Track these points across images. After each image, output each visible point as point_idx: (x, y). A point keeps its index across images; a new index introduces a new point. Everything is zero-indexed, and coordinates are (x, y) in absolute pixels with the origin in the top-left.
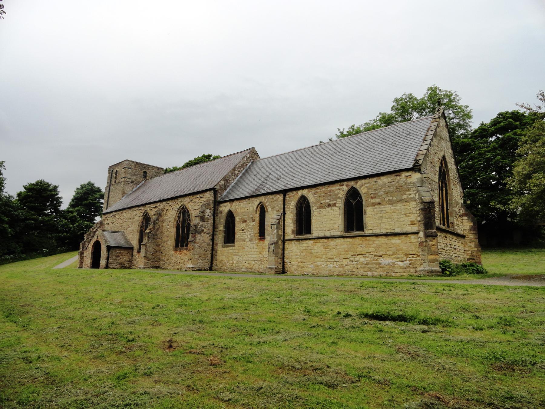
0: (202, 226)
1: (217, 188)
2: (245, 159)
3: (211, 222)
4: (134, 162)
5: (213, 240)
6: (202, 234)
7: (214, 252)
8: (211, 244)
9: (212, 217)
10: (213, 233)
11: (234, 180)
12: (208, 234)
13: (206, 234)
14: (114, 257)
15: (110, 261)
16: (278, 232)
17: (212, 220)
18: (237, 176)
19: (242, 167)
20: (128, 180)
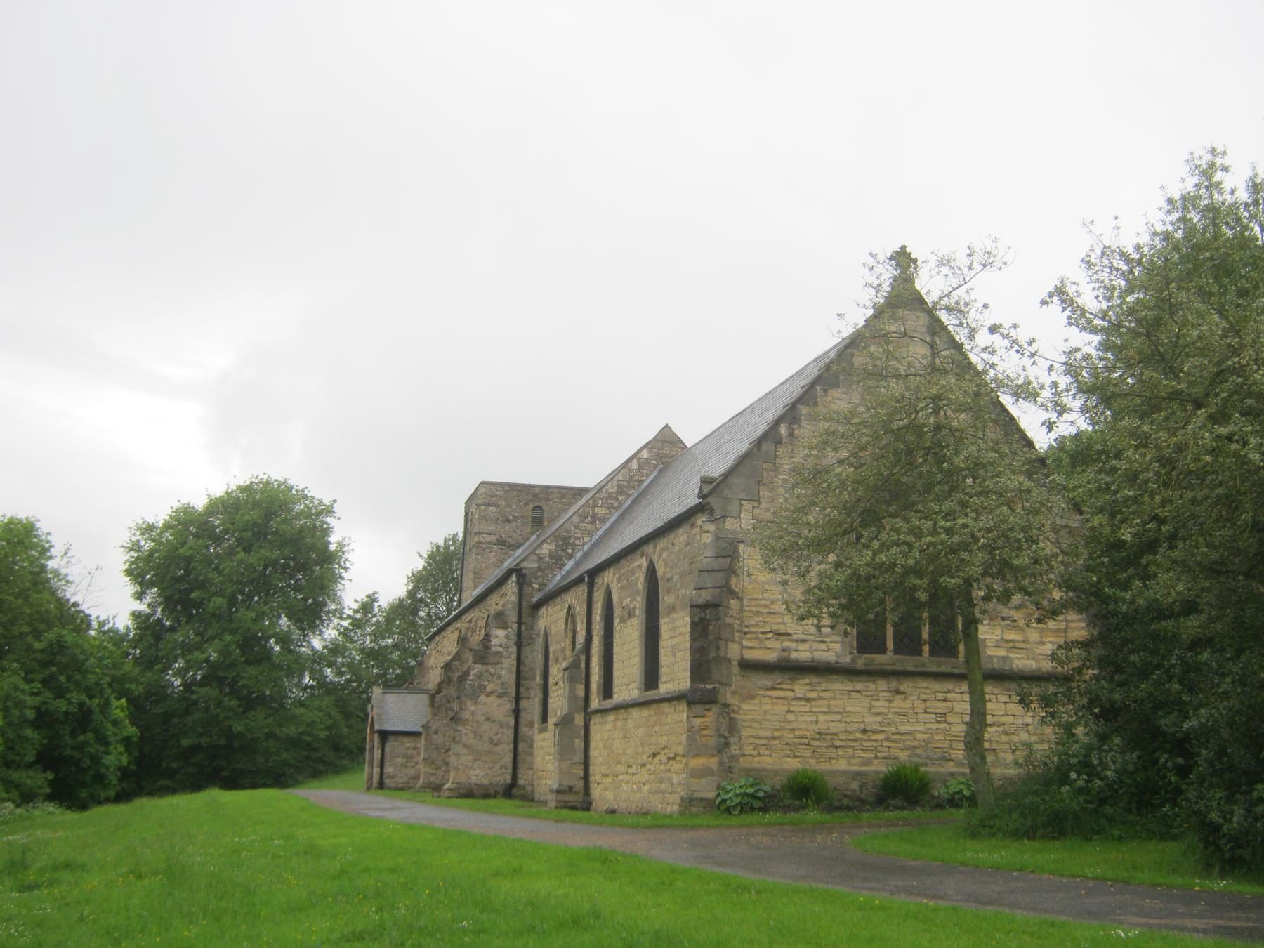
0: (479, 676)
1: (531, 565)
2: (635, 465)
3: (509, 663)
4: (502, 485)
5: (517, 713)
6: (483, 698)
7: (521, 746)
8: (512, 723)
9: (514, 649)
10: (518, 692)
11: (590, 534)
12: (500, 696)
13: (492, 698)
14: (400, 760)
15: (389, 769)
16: (572, 690)
17: (514, 656)
18: (603, 521)
19: (621, 493)
20: (488, 538)
